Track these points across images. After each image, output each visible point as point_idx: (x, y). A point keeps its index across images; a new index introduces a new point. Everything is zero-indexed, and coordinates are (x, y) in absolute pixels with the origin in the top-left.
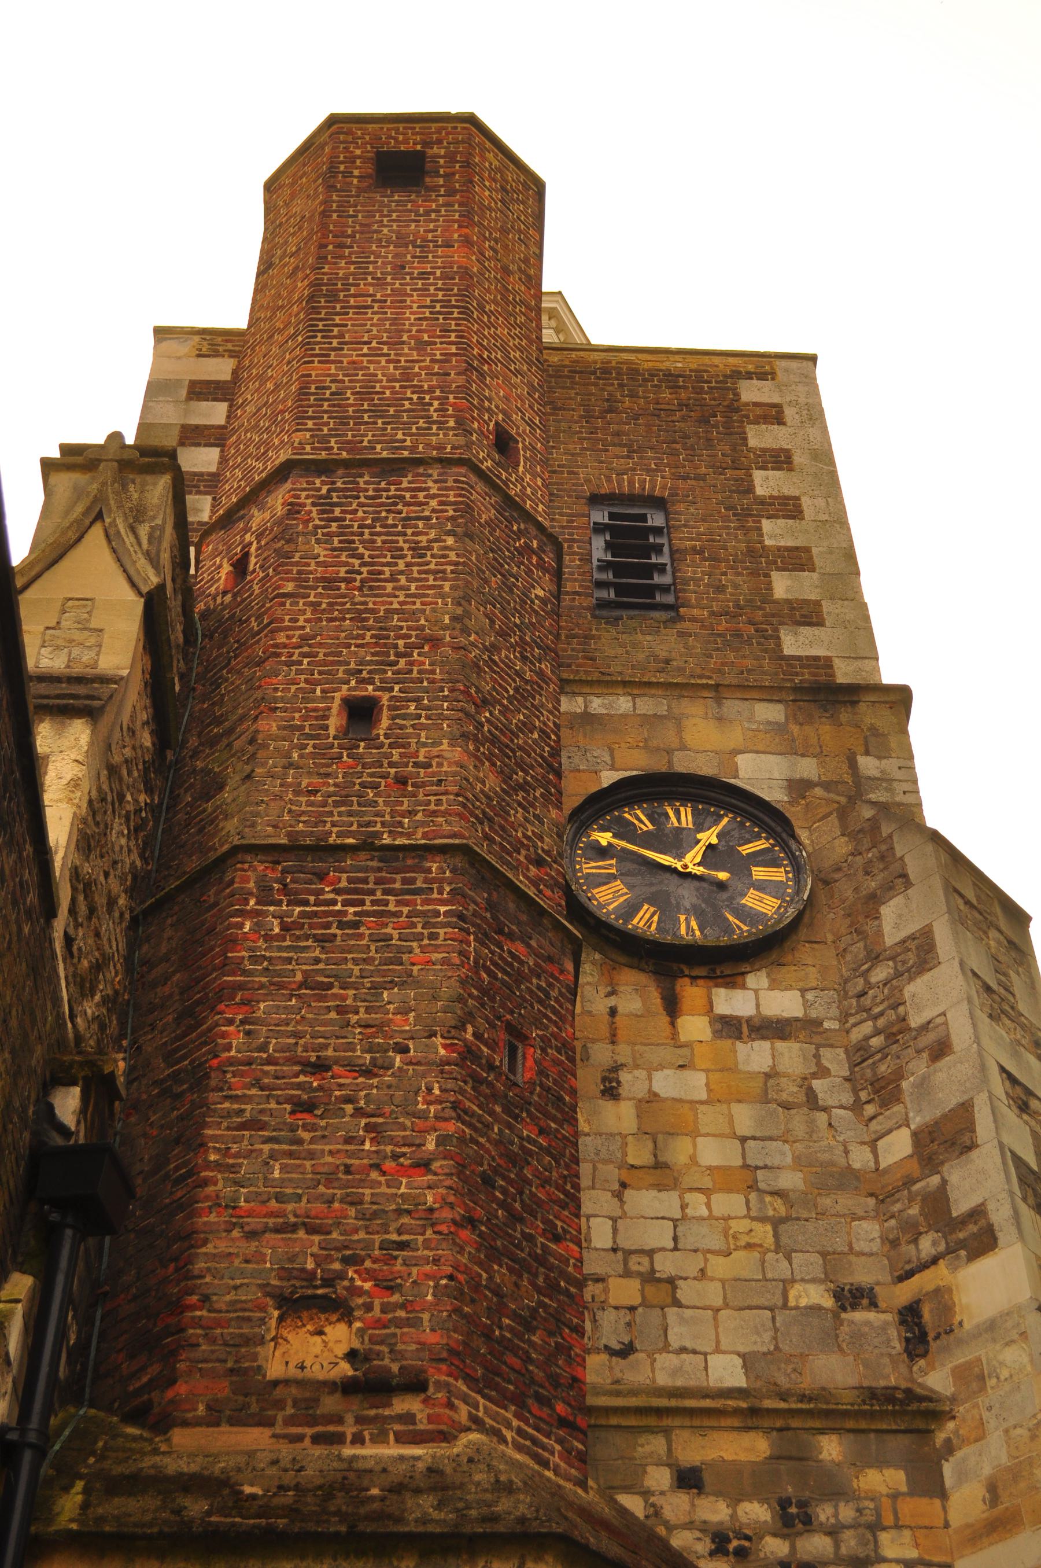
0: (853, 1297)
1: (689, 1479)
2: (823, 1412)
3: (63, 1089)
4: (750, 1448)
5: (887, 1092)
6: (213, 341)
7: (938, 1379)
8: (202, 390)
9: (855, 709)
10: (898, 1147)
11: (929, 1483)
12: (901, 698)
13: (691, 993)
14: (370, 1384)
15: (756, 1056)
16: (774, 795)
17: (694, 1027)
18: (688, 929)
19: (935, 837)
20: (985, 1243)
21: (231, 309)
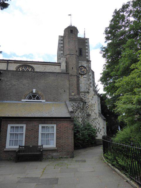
0: (87, 88)
1: (82, 94)
2: (86, 92)
3: (107, 124)
4: (84, 93)
5: (89, 80)
6: (62, 37)
7: (89, 91)
8: (62, 40)
9: (89, 61)
10: (89, 83)
11: (89, 95)
12: (91, 61)
13: (82, 76)
14: (75, 95)
15: (84, 79)
16: (68, 115)
17: (82, 77)
18: (82, 73)
19: (92, 71)
20: (91, 87)
21: (62, 35)
